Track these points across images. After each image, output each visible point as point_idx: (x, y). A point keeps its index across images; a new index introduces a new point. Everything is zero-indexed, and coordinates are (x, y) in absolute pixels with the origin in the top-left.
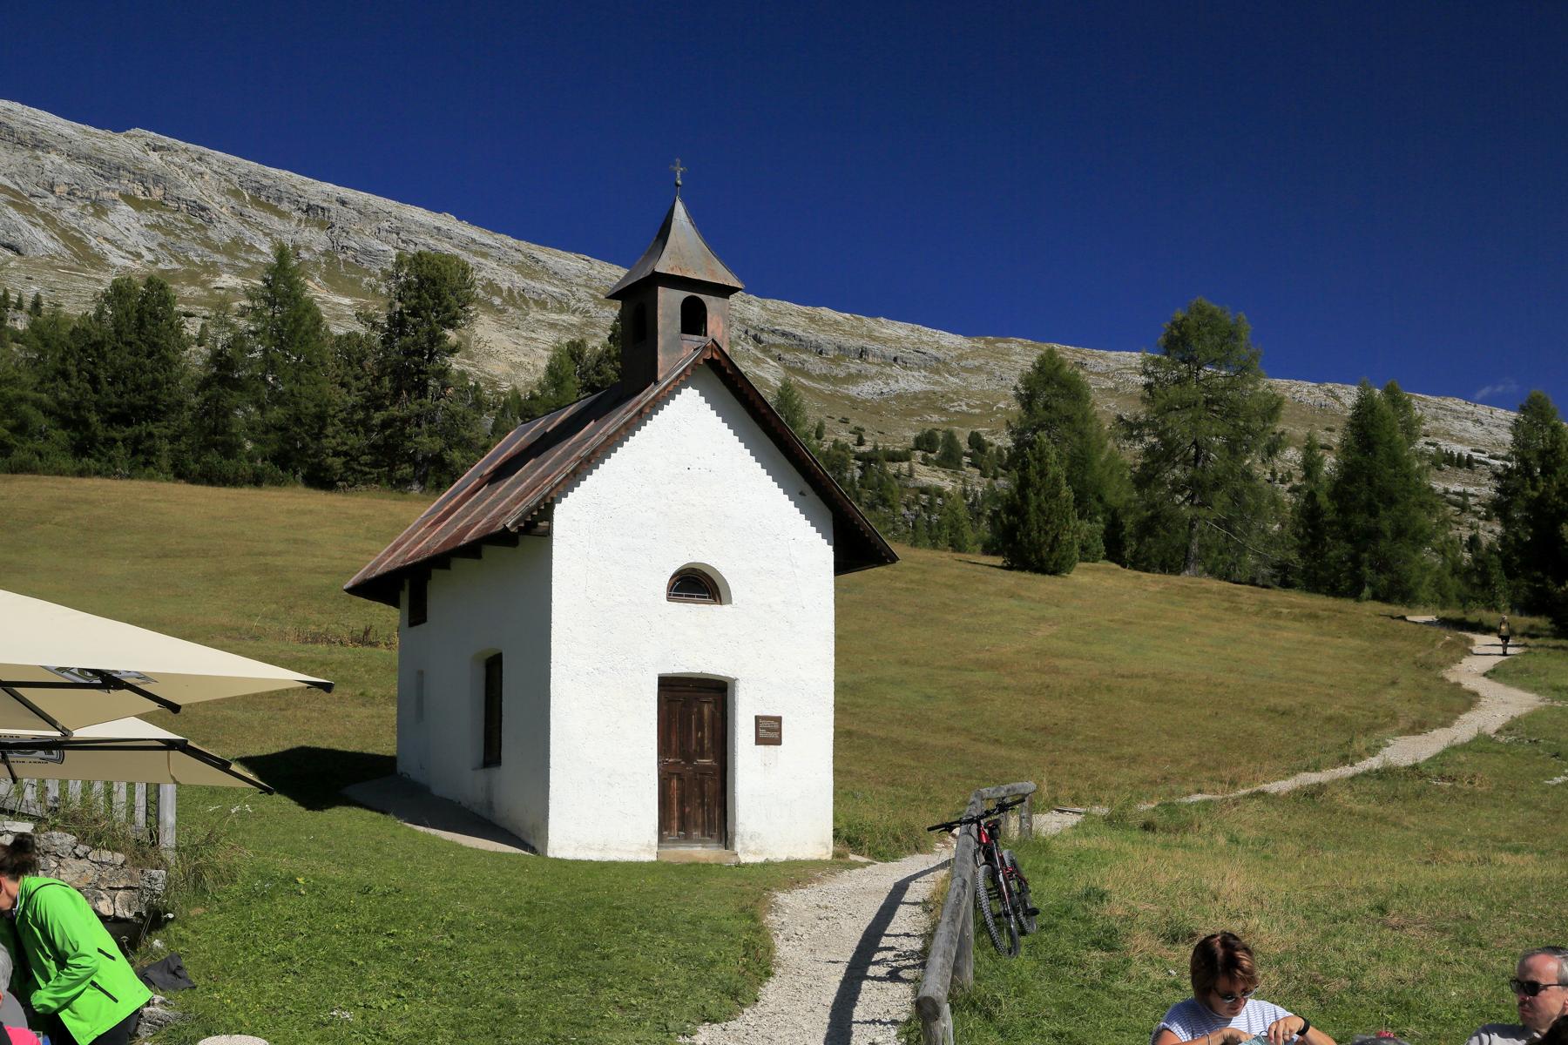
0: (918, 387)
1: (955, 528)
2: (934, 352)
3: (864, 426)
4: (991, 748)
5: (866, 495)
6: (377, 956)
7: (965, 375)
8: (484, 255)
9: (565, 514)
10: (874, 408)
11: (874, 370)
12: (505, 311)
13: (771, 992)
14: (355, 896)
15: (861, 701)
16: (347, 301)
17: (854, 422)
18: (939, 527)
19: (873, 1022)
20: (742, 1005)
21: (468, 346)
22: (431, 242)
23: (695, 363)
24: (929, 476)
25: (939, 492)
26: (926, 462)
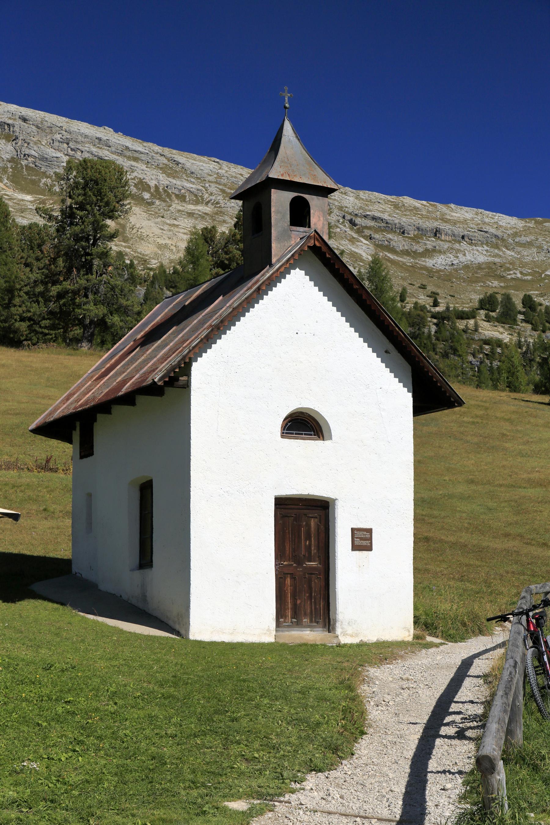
0: (482, 259)
1: (512, 373)
2: (493, 230)
3: (439, 291)
4: (540, 550)
5: (440, 346)
6: (58, 719)
7: (519, 249)
8: (136, 159)
9: (201, 371)
10: (446, 277)
11: (446, 246)
12: (153, 203)
13: (364, 748)
14: (40, 671)
15: (436, 513)
16: (29, 198)
17: (431, 288)
18: (499, 373)
19: (444, 772)
20: (341, 758)
21: (124, 232)
22: (94, 150)
23: (301, 249)
24: (490, 331)
25: (499, 343)
26: (488, 319)
